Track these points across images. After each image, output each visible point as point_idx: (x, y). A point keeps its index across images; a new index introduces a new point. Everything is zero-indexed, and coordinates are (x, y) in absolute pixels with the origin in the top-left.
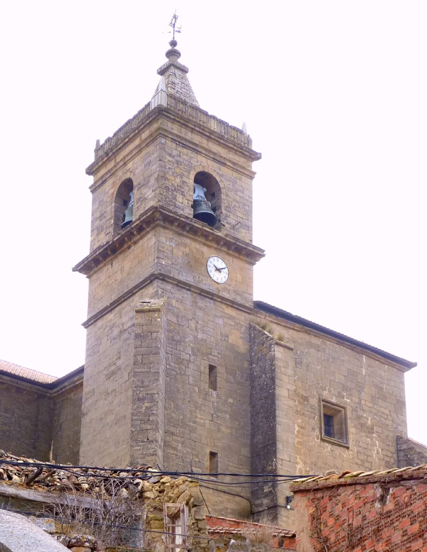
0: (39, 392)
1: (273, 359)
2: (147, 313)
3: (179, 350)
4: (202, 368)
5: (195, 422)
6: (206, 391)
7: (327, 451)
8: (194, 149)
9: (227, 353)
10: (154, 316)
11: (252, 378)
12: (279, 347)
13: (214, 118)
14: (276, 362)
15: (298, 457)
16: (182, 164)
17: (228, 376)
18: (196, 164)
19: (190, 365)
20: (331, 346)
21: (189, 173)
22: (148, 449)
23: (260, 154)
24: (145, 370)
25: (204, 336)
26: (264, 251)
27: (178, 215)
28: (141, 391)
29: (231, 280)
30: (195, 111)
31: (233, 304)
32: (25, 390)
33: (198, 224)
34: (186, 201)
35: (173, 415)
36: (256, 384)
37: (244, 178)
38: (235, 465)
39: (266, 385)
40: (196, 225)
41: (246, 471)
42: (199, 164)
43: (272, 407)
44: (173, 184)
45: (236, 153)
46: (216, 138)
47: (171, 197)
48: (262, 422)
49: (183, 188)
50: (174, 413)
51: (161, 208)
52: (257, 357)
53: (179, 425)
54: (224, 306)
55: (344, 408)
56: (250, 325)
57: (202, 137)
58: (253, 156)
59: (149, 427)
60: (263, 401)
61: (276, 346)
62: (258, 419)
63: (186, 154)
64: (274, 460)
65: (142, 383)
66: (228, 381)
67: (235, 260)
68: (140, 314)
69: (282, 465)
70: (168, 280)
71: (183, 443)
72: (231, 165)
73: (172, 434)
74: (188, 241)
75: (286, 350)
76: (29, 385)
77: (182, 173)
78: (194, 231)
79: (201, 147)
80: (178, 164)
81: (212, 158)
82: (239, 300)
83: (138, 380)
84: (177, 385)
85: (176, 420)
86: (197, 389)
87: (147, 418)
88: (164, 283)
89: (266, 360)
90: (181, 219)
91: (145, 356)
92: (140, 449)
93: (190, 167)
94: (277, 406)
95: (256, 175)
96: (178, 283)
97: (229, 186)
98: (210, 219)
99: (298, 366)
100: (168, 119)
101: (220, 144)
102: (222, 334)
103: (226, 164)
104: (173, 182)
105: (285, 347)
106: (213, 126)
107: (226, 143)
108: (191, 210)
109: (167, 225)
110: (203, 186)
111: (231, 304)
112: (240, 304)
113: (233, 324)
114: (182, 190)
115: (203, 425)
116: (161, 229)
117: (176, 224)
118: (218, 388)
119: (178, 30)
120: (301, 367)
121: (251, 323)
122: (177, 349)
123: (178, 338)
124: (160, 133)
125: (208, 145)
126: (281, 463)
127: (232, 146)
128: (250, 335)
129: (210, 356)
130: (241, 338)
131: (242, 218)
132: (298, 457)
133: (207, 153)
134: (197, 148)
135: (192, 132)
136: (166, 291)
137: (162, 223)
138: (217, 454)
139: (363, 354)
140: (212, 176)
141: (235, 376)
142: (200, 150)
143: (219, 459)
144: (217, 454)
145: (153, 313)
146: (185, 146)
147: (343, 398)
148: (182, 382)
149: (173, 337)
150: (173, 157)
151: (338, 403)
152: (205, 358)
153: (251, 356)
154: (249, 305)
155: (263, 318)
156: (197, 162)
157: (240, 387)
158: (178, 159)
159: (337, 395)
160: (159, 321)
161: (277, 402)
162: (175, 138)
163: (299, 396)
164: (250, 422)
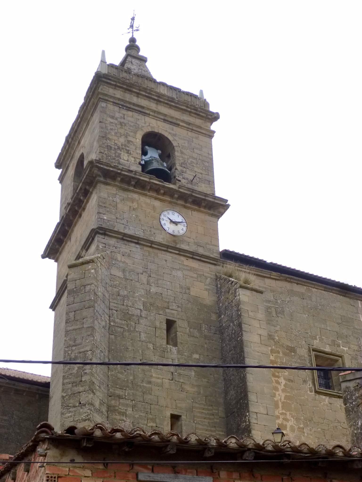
0: (40, 392)
1: (238, 304)
2: (81, 267)
3: (127, 306)
4: (158, 324)
5: (150, 383)
6: (164, 348)
7: (324, 404)
8: (140, 112)
9: (189, 306)
10: (87, 269)
11: (221, 330)
12: (244, 290)
13: (164, 84)
14: (241, 306)
15: (288, 413)
16: (127, 125)
17: (191, 330)
18: (143, 125)
19: (141, 321)
20: (317, 294)
21: (135, 133)
22: (80, 414)
23: (218, 114)
24: (77, 327)
25: (159, 290)
26: (227, 201)
27: (119, 169)
28: (72, 351)
29: (191, 232)
30: (140, 78)
31: (193, 255)
32: (24, 391)
33: (145, 178)
34: (133, 159)
35: (120, 376)
36: (225, 335)
37: (201, 137)
38: (205, 427)
39: (234, 334)
40: (142, 178)
41: (221, 433)
42: (147, 124)
43: (241, 356)
44: (116, 143)
45: (190, 115)
46: (166, 101)
47: (114, 155)
48: (233, 375)
49: (128, 147)
50: (122, 373)
51: (98, 163)
52: (224, 307)
53: (128, 387)
54: (182, 258)
55: (341, 357)
56: (216, 276)
57: (149, 101)
58: (210, 117)
59: (81, 389)
60: (233, 352)
61: (240, 289)
62: (229, 373)
63: (131, 117)
64: (247, 414)
65: (74, 342)
66: (191, 335)
67: (195, 213)
68: (73, 269)
69: (257, 419)
70: (110, 234)
71: (133, 407)
72: (185, 125)
73: (119, 397)
74: (136, 196)
75: (254, 293)
76: (28, 385)
77: (127, 133)
78: (140, 186)
79: (148, 109)
80: (122, 125)
81: (162, 119)
82: (201, 251)
83: (70, 340)
84: (124, 343)
85: (124, 381)
86: (151, 346)
87: (79, 379)
88: (106, 237)
89: (232, 307)
90: (123, 173)
91: (78, 312)
92: (71, 416)
93: (137, 128)
94: (246, 354)
95: (215, 134)
96: (124, 236)
97: (183, 144)
98: (164, 175)
99: (279, 315)
100: (109, 86)
101: (171, 107)
102: (181, 287)
103: (179, 125)
104: (116, 142)
105: (252, 290)
106: (163, 91)
107: (178, 105)
108: (138, 167)
109: (109, 181)
110: (157, 149)
111: (191, 256)
112: (202, 255)
113: (195, 276)
114: (127, 148)
115: (161, 385)
116: (102, 186)
117: (119, 179)
118: (178, 343)
119: (136, 29)
120: (283, 317)
121: (217, 274)
122: (123, 305)
123: (126, 293)
124: (100, 98)
125: (157, 108)
126: (255, 416)
127: (184, 108)
128: (217, 286)
129: (167, 310)
130: (206, 290)
131: (202, 174)
132: (288, 413)
133: (156, 115)
134: (143, 110)
135: (138, 97)
136: (109, 245)
137: (102, 179)
138: (180, 416)
139: (357, 300)
140: (163, 136)
141: (200, 330)
142: (148, 112)
143: (183, 422)
144: (181, 416)
145: (86, 265)
146: (129, 109)
147: (339, 346)
148: (132, 340)
149: (119, 291)
150: (116, 119)
151: (333, 352)
152: (161, 312)
153: (219, 307)
154: (215, 255)
155: (231, 266)
156: (145, 123)
157: (207, 341)
158: (122, 120)
159: (330, 343)
160: (92, 273)
161: (246, 349)
162: (117, 101)
163: (283, 347)
164: (222, 378)
